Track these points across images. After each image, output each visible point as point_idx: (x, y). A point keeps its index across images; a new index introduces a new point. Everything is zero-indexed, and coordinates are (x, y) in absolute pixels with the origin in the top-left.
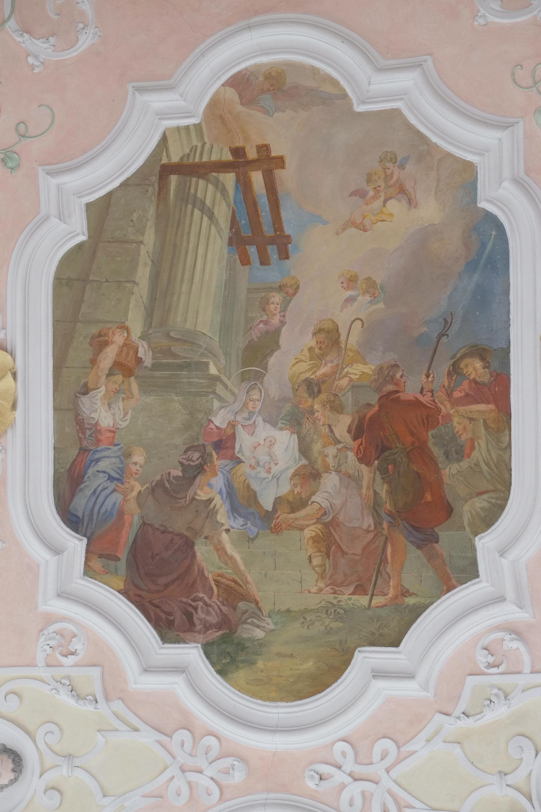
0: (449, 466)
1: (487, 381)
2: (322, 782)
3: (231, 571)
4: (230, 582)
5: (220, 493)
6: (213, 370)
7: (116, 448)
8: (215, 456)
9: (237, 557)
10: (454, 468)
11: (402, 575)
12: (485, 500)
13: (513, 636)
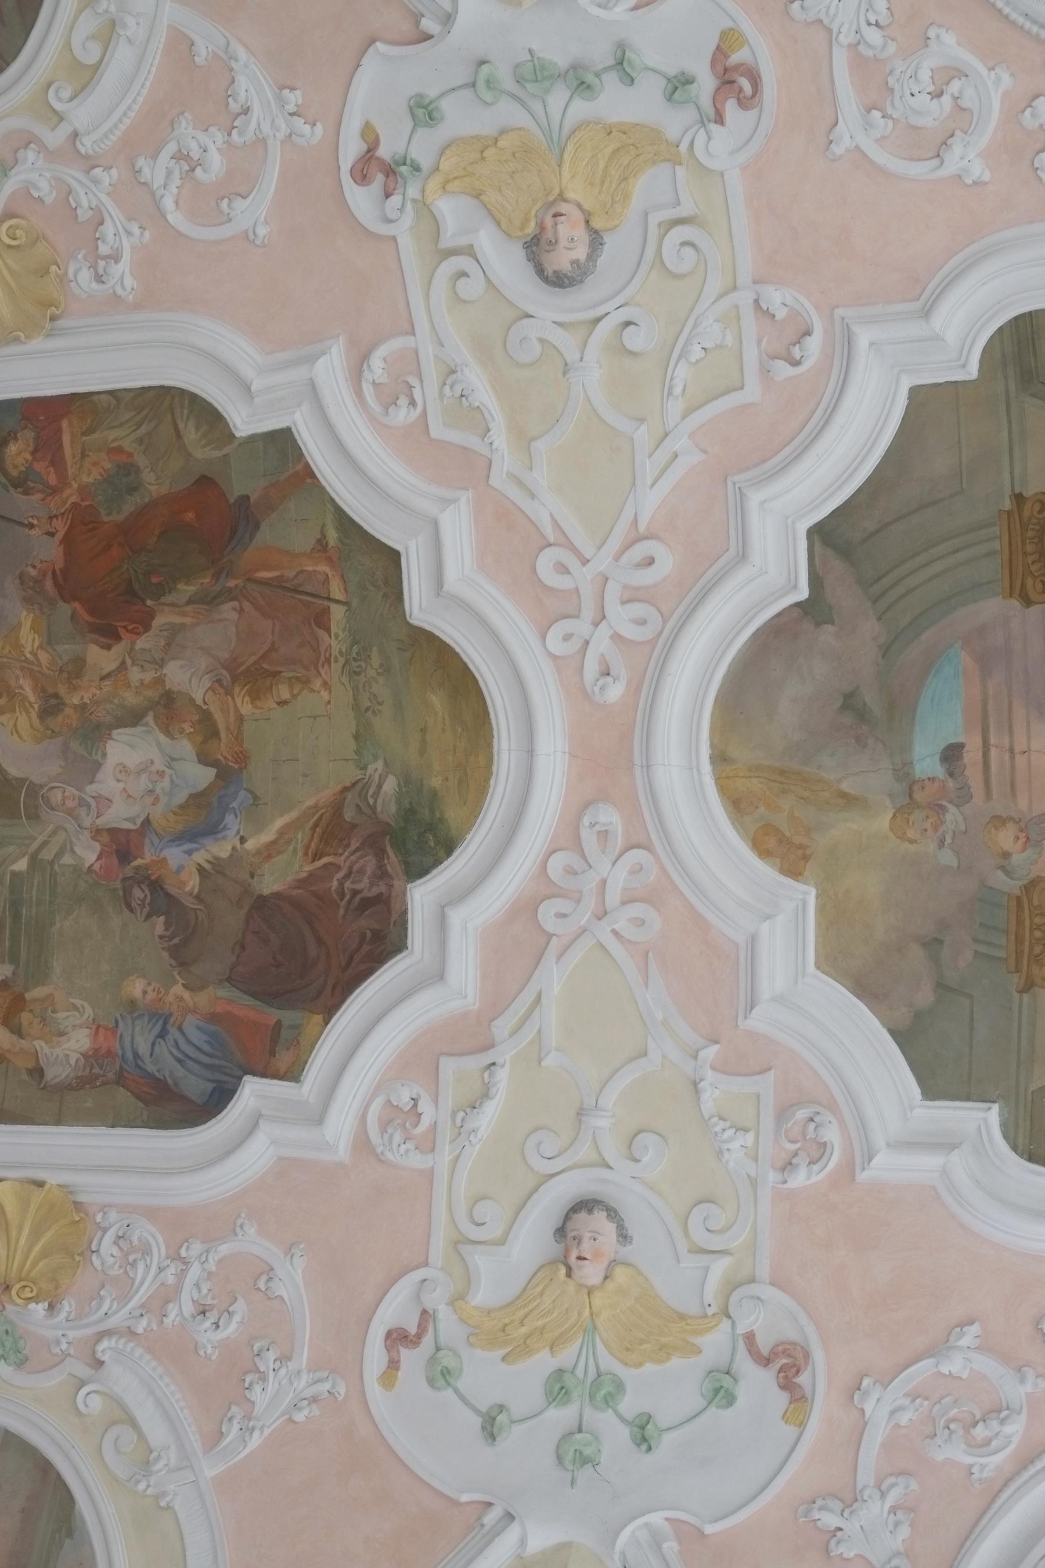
0: (147, 486)
1: (33, 434)
2: (611, 673)
3: (300, 833)
4: (315, 835)
5: (189, 853)
6: (22, 865)
7: (121, 1025)
8: (138, 862)
9: (279, 823)
10: (148, 477)
11: (297, 551)
12: (186, 425)
13: (365, 366)
